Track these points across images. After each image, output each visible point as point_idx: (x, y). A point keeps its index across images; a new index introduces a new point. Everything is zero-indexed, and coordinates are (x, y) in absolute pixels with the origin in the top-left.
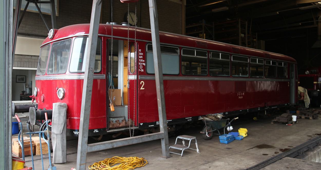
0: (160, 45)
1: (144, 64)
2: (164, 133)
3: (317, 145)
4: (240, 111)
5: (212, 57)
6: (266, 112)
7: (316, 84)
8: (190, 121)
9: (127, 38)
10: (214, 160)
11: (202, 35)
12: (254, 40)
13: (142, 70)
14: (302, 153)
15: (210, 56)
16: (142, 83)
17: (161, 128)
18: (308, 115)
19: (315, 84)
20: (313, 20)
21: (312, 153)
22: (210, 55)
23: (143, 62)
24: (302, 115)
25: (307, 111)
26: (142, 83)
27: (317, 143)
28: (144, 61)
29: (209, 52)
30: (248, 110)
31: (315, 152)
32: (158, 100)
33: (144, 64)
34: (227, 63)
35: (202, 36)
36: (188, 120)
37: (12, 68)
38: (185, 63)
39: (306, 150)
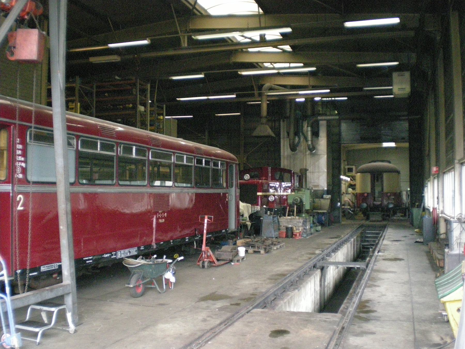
0: (66, 134)
1: (23, 165)
2: (71, 283)
3: (284, 291)
4: (161, 243)
5: (123, 153)
6: (195, 244)
7: (260, 195)
8: (90, 263)
9: (14, 121)
10: (156, 322)
11: (74, 104)
12: (159, 117)
13: (21, 176)
14: (270, 302)
15: (120, 151)
16: (20, 199)
17: (66, 277)
18: (258, 248)
19: (259, 196)
20: (254, 90)
21: (282, 302)
22: (119, 149)
23: (21, 161)
24: (249, 246)
25: (255, 240)
26: (20, 199)
27: (284, 288)
28: (23, 159)
29: (118, 144)
30: (171, 241)
31: (286, 300)
32: (61, 227)
33: (23, 165)
34: (142, 163)
35: (74, 107)
36: (87, 262)
39: (273, 298)
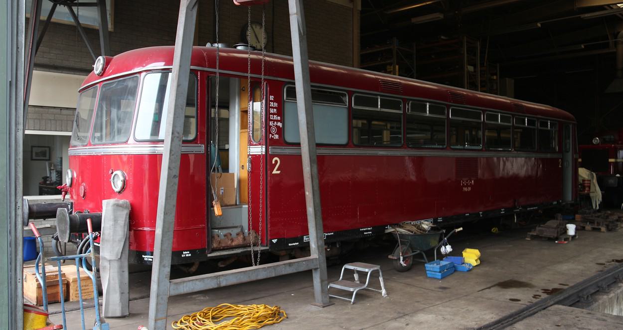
0: (310, 86)
1: (280, 124)
2: (319, 257)
3: (615, 282)
4: (467, 215)
5: (411, 111)
6: (515, 217)
7: (613, 162)
8: (369, 234)
9: (246, 74)
10: (416, 311)
11: (392, 67)
12: (492, 77)
13: (276, 137)
14: (585, 297)
15: (408, 109)
16: (276, 161)
17: (313, 249)
18: (598, 224)
19: (611, 162)
20: (608, 39)
21: (605, 297)
22: (407, 107)
23: (277, 121)
24: (587, 222)
25: (596, 215)
26: (276, 161)
27: (616, 278)
28: (279, 118)
29: (405, 101)
30: (481, 213)
31: (612, 295)
32: (307, 193)
33: (280, 124)
34: (440, 123)
35: (392, 70)
36: (365, 233)
37: (24, 132)
38: (358, 123)
39: (593, 291)
